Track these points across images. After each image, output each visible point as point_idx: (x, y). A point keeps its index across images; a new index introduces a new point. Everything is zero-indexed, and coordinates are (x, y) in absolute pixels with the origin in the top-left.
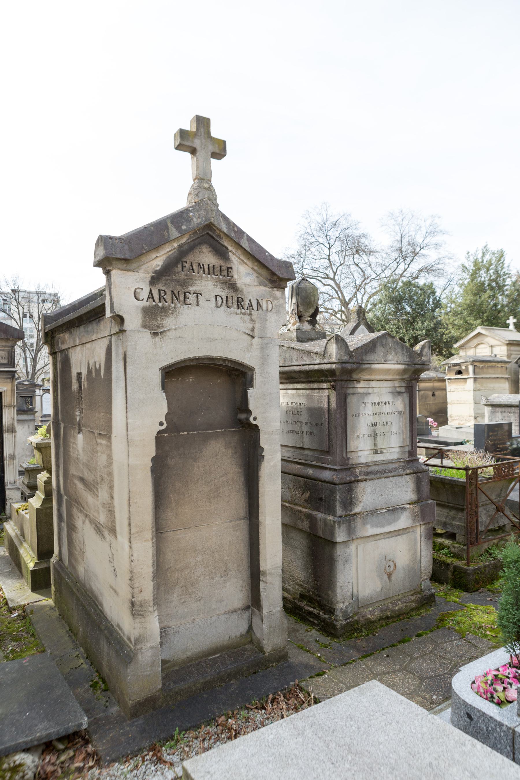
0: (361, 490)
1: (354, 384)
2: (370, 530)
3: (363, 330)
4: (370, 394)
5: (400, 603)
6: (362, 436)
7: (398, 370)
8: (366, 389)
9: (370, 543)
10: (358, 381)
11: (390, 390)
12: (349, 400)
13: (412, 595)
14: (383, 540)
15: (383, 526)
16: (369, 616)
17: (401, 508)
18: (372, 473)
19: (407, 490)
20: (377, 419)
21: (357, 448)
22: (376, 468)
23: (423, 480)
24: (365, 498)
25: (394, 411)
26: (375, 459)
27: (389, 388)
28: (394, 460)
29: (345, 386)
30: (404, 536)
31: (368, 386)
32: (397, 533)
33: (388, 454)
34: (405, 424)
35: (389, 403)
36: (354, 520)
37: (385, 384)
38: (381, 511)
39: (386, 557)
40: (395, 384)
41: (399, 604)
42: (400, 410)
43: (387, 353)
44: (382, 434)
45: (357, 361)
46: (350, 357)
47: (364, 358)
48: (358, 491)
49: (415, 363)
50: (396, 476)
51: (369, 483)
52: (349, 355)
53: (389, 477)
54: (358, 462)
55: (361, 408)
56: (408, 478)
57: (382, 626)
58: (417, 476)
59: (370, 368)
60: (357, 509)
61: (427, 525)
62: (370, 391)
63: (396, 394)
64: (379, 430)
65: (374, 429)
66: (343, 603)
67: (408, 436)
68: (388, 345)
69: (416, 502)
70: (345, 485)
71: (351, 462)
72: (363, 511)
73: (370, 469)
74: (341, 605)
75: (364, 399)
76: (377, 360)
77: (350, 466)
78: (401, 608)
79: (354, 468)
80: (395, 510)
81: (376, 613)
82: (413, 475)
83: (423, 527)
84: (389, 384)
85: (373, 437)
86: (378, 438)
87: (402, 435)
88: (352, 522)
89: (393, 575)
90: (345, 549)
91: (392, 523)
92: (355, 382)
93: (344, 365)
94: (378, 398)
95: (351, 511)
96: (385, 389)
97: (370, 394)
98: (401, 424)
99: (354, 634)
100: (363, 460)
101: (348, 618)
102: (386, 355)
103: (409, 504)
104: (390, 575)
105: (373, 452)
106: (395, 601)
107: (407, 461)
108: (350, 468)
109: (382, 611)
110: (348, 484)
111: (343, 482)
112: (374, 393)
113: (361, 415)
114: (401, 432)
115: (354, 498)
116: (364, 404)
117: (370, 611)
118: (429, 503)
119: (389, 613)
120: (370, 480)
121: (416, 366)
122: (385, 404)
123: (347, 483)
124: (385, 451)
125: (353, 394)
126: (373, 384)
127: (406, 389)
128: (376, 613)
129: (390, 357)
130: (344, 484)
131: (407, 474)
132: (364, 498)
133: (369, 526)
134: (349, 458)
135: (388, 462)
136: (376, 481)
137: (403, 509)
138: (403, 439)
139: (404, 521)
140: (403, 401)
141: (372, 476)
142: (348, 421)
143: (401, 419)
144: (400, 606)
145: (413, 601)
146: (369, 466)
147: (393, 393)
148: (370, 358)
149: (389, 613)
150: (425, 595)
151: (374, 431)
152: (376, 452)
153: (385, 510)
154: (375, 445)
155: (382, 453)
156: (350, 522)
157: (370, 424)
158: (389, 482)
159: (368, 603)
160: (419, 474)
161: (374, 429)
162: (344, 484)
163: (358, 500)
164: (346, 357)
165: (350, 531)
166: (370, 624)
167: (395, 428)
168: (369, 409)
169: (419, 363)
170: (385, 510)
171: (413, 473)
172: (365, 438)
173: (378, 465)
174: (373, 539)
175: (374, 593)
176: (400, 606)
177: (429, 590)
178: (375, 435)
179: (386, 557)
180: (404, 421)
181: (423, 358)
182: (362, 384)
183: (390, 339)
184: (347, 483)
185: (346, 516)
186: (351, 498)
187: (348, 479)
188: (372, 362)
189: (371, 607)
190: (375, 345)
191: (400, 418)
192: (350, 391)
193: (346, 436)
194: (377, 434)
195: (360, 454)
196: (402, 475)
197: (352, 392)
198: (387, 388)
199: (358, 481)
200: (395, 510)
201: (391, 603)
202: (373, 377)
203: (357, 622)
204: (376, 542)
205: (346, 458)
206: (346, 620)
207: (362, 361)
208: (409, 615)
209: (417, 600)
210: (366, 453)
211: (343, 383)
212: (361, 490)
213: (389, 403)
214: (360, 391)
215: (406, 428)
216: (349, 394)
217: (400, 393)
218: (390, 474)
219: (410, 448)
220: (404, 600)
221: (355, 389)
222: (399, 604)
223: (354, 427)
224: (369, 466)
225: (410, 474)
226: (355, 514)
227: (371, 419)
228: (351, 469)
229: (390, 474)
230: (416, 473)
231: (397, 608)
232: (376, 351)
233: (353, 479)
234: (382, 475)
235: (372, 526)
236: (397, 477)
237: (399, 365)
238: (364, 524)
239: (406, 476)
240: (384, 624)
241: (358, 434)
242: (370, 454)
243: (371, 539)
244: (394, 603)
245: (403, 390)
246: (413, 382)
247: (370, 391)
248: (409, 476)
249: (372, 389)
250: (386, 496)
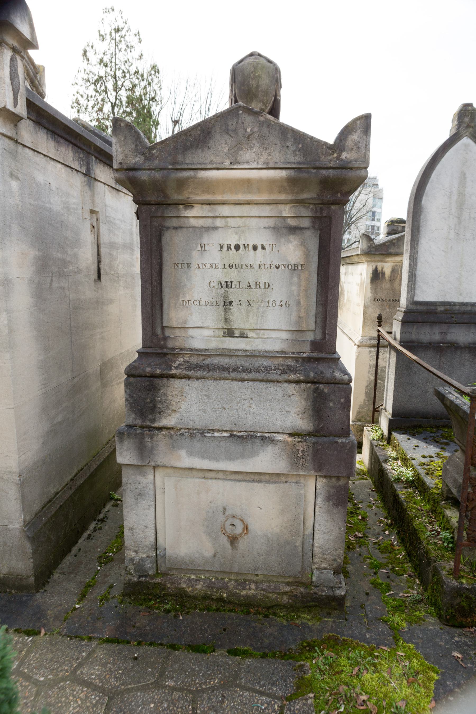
0: (175, 393)
1: (179, 210)
2: (185, 459)
3: (466, 146)
4: (216, 228)
5: (253, 586)
6: (197, 303)
7: (281, 180)
8: (210, 220)
9: (190, 480)
10: (189, 205)
11: (271, 223)
12: (166, 238)
13: (288, 584)
14: (220, 482)
15: (216, 459)
16: (184, 586)
17: (263, 438)
18: (207, 368)
19: (287, 409)
20: (233, 276)
21: (185, 323)
22: (225, 361)
23: (332, 397)
24: (183, 406)
25: (276, 263)
26: (226, 346)
27: (266, 220)
28: (272, 352)
29: (159, 214)
30: (271, 487)
31: (211, 215)
32: (257, 477)
33: (258, 341)
34: (306, 291)
35: (263, 248)
36: (152, 437)
37: (254, 211)
38: (216, 434)
39: (225, 509)
40: (281, 212)
41: (250, 589)
42: (293, 262)
43: (238, 147)
44: (245, 304)
45: (162, 165)
46: (147, 159)
47: (180, 158)
48: (169, 393)
49: (317, 164)
50: (261, 381)
51: (195, 384)
52: (143, 154)
53: (243, 380)
54: (187, 346)
55: (195, 254)
56: (291, 388)
57: (208, 609)
58: (316, 389)
59: (195, 178)
60: (168, 421)
61: (334, 480)
62: (218, 223)
63: (284, 231)
64: (235, 295)
65: (226, 293)
66: (136, 552)
67: (313, 312)
68: (241, 132)
69: (310, 434)
70: (139, 379)
71: (170, 344)
72: (179, 427)
73: (208, 361)
74: (133, 554)
75: (201, 237)
76: (211, 162)
77: (165, 351)
78: (253, 595)
79: (176, 355)
80: (247, 438)
81: (199, 587)
82: (303, 385)
83: (322, 482)
84: (267, 211)
85: (221, 307)
86: (234, 309)
87: (295, 308)
88: (147, 440)
89: (241, 541)
90: (139, 477)
91: (237, 458)
92: (181, 207)
93: (131, 174)
94: (236, 237)
95: (153, 421)
96: (257, 220)
97: (216, 228)
98: (294, 288)
99: (151, 600)
100: (197, 344)
101: (146, 576)
102: (236, 152)
103: (291, 435)
104: (233, 540)
105: (221, 333)
106: (246, 580)
107: (304, 358)
108: (165, 354)
109: (211, 586)
110: (147, 379)
111: (137, 373)
112: (227, 227)
113: (194, 266)
114: (292, 303)
115: (160, 402)
116: (203, 246)
117: (189, 579)
118: (336, 443)
119: (225, 595)
120: (198, 379)
121: (324, 172)
122: (255, 248)
123: (146, 376)
124: (250, 334)
125: (176, 228)
126: (225, 210)
127: (313, 223)
128: (199, 587)
129: (247, 155)
130: (140, 376)
131: (289, 382)
132: (183, 407)
133: (183, 453)
134: (169, 337)
135: (254, 355)
136: (209, 382)
137: (272, 441)
138: (300, 317)
139: (266, 460)
140: (303, 244)
141: (200, 373)
142: (165, 276)
143: (295, 280)
144: (252, 591)
145: (285, 593)
146: (209, 356)
147: (275, 229)
148: (196, 157)
149: (225, 595)
150: (316, 593)
151: (225, 296)
152: (230, 333)
153: (225, 434)
154: (226, 321)
155: (243, 336)
156: (144, 439)
157: (215, 284)
158: (244, 390)
159: (184, 567)
160: (322, 386)
161: (226, 293)
162: (140, 376)
163: (168, 407)
164: (137, 159)
165: (143, 451)
166: (183, 600)
167: (278, 294)
168: (213, 256)
169: (332, 164)
170: (225, 434)
171: (306, 382)
172: (203, 307)
173: (230, 356)
174: (201, 474)
175: (197, 555)
176: (252, 592)
177: (332, 588)
178: (227, 304)
179: (225, 509)
180: (303, 283)
181: (344, 155)
182: (196, 211)
183: (248, 119)
184: (146, 376)
185: (142, 427)
186: (153, 401)
187: (148, 369)
188: (199, 166)
189: (195, 574)
190: (209, 133)
191: (291, 277)
192: (169, 223)
193: (161, 299)
194: (231, 303)
195: (191, 332)
196: (278, 382)
197: (175, 225)
198: (262, 220)
199: (173, 377)
200: (247, 438)
201: (236, 581)
202: (219, 198)
203: (162, 587)
204: (203, 480)
205: (161, 336)
206: (140, 576)
207: (173, 164)
208: (271, 611)
209: (296, 596)
210: (207, 333)
211: (153, 208)
212: (175, 393)
213: (263, 248)
214: (193, 222)
215: (307, 296)
216: (168, 228)
217: (293, 230)
218: (244, 375)
219: (319, 336)
220: (265, 585)
221: (182, 220)
222: (250, 589)
223: (178, 288)
224: (209, 356)
225: (298, 382)
226: (160, 429)
227: (219, 275)
228: (169, 356)
229: (244, 375)
230: (313, 382)
231: (243, 593)
232: (211, 144)
233: (158, 371)
234: (226, 375)
235: (191, 454)
236: (264, 384)
237: (278, 171)
238: (173, 446)
239: (286, 385)
240: (214, 607)
241: (187, 299)
242: (215, 336)
243: (195, 473)
244: (243, 584)
245: (306, 223)
246: (333, 207)
247: (218, 223)
248: (293, 385)
249: (223, 220)
250: (234, 412)
